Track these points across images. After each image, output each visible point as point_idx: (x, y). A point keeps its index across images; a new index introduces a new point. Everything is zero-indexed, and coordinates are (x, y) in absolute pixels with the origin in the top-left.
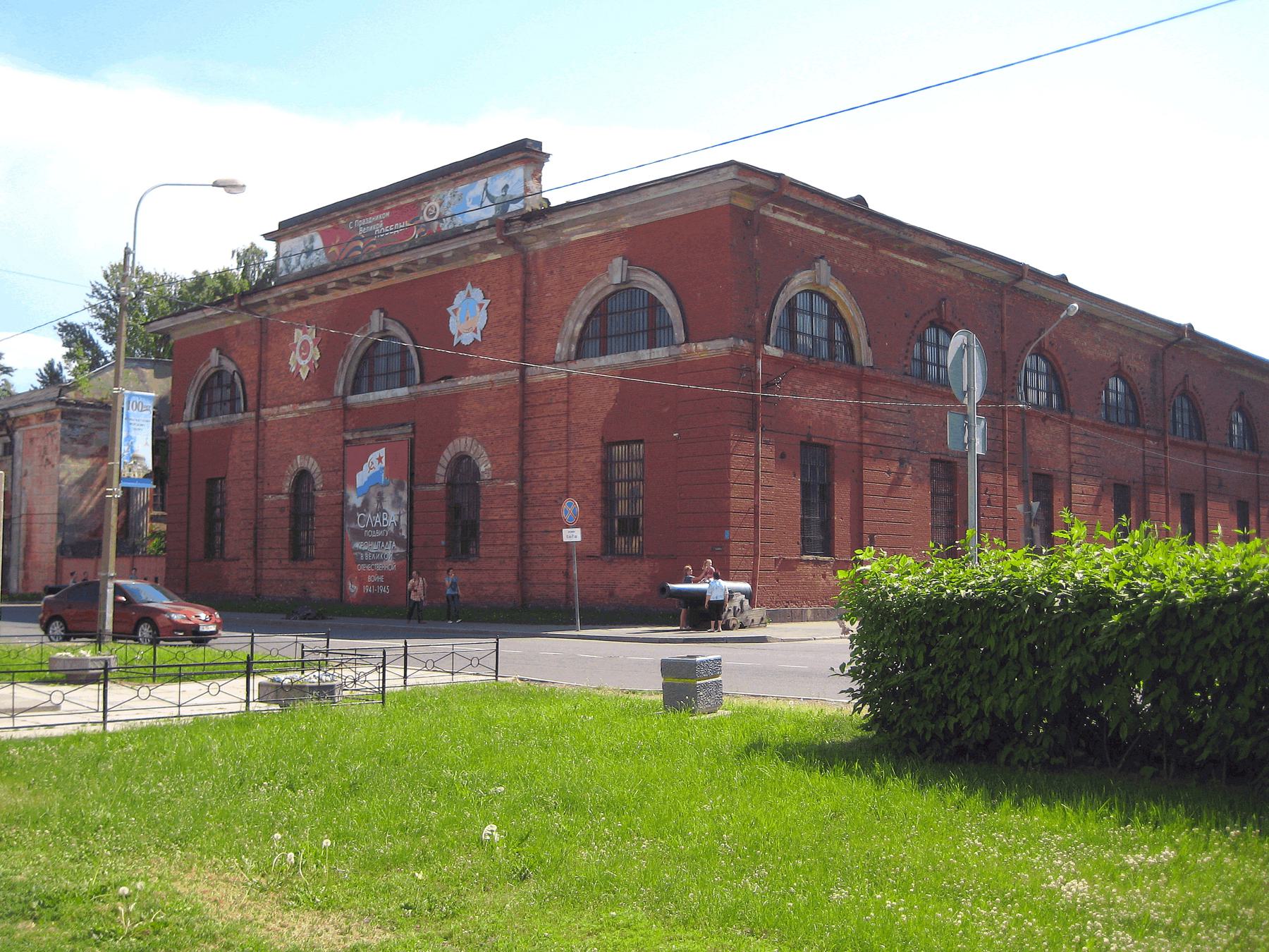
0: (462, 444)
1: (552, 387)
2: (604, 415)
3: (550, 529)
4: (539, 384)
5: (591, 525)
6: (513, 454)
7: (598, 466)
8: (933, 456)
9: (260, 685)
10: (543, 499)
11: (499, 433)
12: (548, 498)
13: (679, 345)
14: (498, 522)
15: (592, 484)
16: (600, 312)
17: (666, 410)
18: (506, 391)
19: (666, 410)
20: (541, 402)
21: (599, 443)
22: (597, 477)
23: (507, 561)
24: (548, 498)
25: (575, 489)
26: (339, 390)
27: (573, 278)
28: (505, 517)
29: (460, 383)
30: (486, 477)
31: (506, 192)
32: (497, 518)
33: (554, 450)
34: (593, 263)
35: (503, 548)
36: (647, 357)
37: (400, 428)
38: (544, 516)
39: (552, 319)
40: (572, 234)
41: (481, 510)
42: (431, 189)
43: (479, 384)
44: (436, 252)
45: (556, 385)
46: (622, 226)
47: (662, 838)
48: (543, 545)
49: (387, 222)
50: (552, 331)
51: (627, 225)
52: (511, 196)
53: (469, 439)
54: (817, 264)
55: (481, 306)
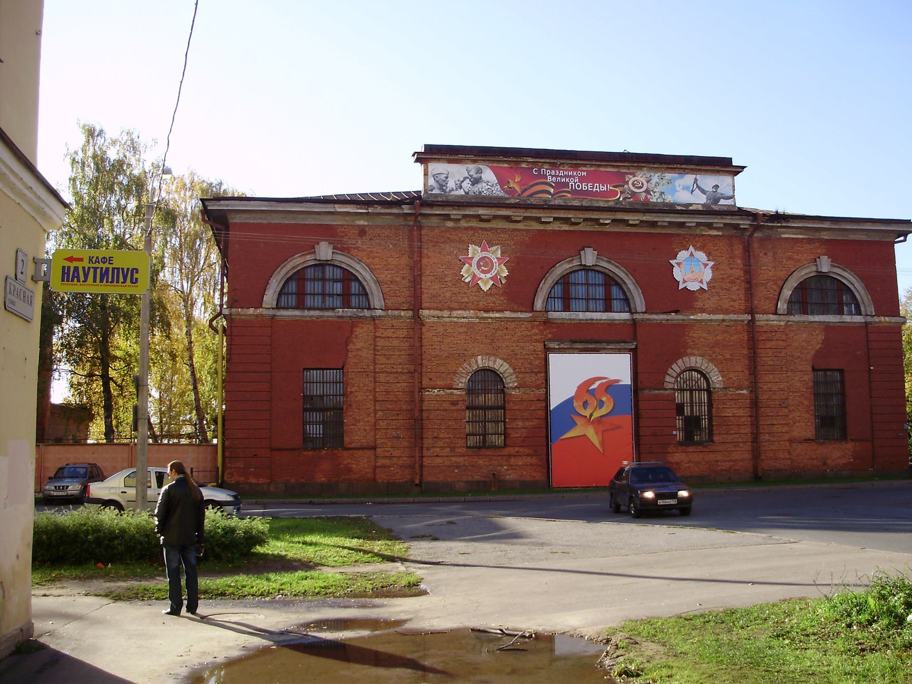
0: (695, 361)
1: (774, 330)
2: (813, 352)
3: (775, 423)
4: (762, 327)
5: (806, 420)
6: (743, 371)
7: (811, 384)
9: (188, 611)
10: (769, 403)
11: (728, 356)
12: (773, 403)
13: (93, 268)
14: (730, 418)
15: (806, 394)
16: (802, 288)
17: (859, 353)
18: (734, 328)
19: (859, 353)
20: (763, 338)
21: (810, 369)
22: (810, 390)
23: (741, 445)
24: (773, 403)
25: (792, 397)
26: (539, 305)
27: (784, 261)
28: (738, 415)
29: (692, 317)
30: (717, 386)
31: (717, 190)
32: (730, 415)
33: (776, 371)
34: (800, 255)
35: (736, 436)
36: (849, 320)
37: (622, 344)
38: (769, 414)
39: (769, 284)
40: (785, 233)
41: (714, 409)
42: (640, 168)
43: (711, 320)
44: (682, 220)
45: (777, 329)
46: (822, 237)
47: (858, 612)
48: (768, 433)
49: (582, 180)
50: (769, 293)
51: (826, 238)
52: (722, 194)
53: (699, 358)
54: (582, 252)
55: (706, 265)
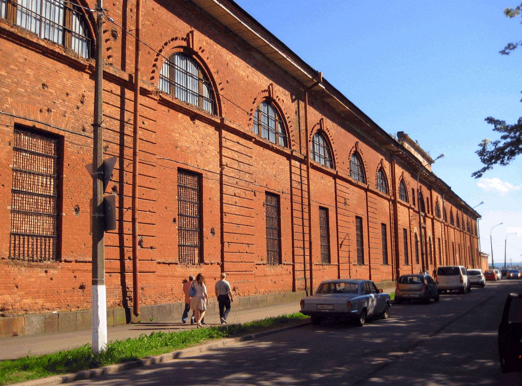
8: (19, 121)
